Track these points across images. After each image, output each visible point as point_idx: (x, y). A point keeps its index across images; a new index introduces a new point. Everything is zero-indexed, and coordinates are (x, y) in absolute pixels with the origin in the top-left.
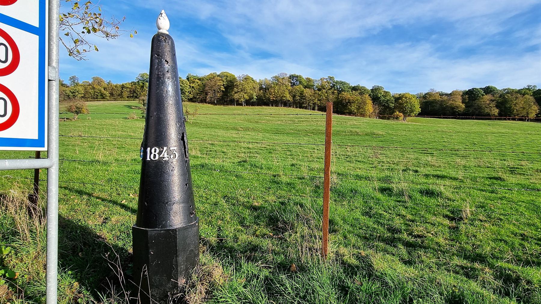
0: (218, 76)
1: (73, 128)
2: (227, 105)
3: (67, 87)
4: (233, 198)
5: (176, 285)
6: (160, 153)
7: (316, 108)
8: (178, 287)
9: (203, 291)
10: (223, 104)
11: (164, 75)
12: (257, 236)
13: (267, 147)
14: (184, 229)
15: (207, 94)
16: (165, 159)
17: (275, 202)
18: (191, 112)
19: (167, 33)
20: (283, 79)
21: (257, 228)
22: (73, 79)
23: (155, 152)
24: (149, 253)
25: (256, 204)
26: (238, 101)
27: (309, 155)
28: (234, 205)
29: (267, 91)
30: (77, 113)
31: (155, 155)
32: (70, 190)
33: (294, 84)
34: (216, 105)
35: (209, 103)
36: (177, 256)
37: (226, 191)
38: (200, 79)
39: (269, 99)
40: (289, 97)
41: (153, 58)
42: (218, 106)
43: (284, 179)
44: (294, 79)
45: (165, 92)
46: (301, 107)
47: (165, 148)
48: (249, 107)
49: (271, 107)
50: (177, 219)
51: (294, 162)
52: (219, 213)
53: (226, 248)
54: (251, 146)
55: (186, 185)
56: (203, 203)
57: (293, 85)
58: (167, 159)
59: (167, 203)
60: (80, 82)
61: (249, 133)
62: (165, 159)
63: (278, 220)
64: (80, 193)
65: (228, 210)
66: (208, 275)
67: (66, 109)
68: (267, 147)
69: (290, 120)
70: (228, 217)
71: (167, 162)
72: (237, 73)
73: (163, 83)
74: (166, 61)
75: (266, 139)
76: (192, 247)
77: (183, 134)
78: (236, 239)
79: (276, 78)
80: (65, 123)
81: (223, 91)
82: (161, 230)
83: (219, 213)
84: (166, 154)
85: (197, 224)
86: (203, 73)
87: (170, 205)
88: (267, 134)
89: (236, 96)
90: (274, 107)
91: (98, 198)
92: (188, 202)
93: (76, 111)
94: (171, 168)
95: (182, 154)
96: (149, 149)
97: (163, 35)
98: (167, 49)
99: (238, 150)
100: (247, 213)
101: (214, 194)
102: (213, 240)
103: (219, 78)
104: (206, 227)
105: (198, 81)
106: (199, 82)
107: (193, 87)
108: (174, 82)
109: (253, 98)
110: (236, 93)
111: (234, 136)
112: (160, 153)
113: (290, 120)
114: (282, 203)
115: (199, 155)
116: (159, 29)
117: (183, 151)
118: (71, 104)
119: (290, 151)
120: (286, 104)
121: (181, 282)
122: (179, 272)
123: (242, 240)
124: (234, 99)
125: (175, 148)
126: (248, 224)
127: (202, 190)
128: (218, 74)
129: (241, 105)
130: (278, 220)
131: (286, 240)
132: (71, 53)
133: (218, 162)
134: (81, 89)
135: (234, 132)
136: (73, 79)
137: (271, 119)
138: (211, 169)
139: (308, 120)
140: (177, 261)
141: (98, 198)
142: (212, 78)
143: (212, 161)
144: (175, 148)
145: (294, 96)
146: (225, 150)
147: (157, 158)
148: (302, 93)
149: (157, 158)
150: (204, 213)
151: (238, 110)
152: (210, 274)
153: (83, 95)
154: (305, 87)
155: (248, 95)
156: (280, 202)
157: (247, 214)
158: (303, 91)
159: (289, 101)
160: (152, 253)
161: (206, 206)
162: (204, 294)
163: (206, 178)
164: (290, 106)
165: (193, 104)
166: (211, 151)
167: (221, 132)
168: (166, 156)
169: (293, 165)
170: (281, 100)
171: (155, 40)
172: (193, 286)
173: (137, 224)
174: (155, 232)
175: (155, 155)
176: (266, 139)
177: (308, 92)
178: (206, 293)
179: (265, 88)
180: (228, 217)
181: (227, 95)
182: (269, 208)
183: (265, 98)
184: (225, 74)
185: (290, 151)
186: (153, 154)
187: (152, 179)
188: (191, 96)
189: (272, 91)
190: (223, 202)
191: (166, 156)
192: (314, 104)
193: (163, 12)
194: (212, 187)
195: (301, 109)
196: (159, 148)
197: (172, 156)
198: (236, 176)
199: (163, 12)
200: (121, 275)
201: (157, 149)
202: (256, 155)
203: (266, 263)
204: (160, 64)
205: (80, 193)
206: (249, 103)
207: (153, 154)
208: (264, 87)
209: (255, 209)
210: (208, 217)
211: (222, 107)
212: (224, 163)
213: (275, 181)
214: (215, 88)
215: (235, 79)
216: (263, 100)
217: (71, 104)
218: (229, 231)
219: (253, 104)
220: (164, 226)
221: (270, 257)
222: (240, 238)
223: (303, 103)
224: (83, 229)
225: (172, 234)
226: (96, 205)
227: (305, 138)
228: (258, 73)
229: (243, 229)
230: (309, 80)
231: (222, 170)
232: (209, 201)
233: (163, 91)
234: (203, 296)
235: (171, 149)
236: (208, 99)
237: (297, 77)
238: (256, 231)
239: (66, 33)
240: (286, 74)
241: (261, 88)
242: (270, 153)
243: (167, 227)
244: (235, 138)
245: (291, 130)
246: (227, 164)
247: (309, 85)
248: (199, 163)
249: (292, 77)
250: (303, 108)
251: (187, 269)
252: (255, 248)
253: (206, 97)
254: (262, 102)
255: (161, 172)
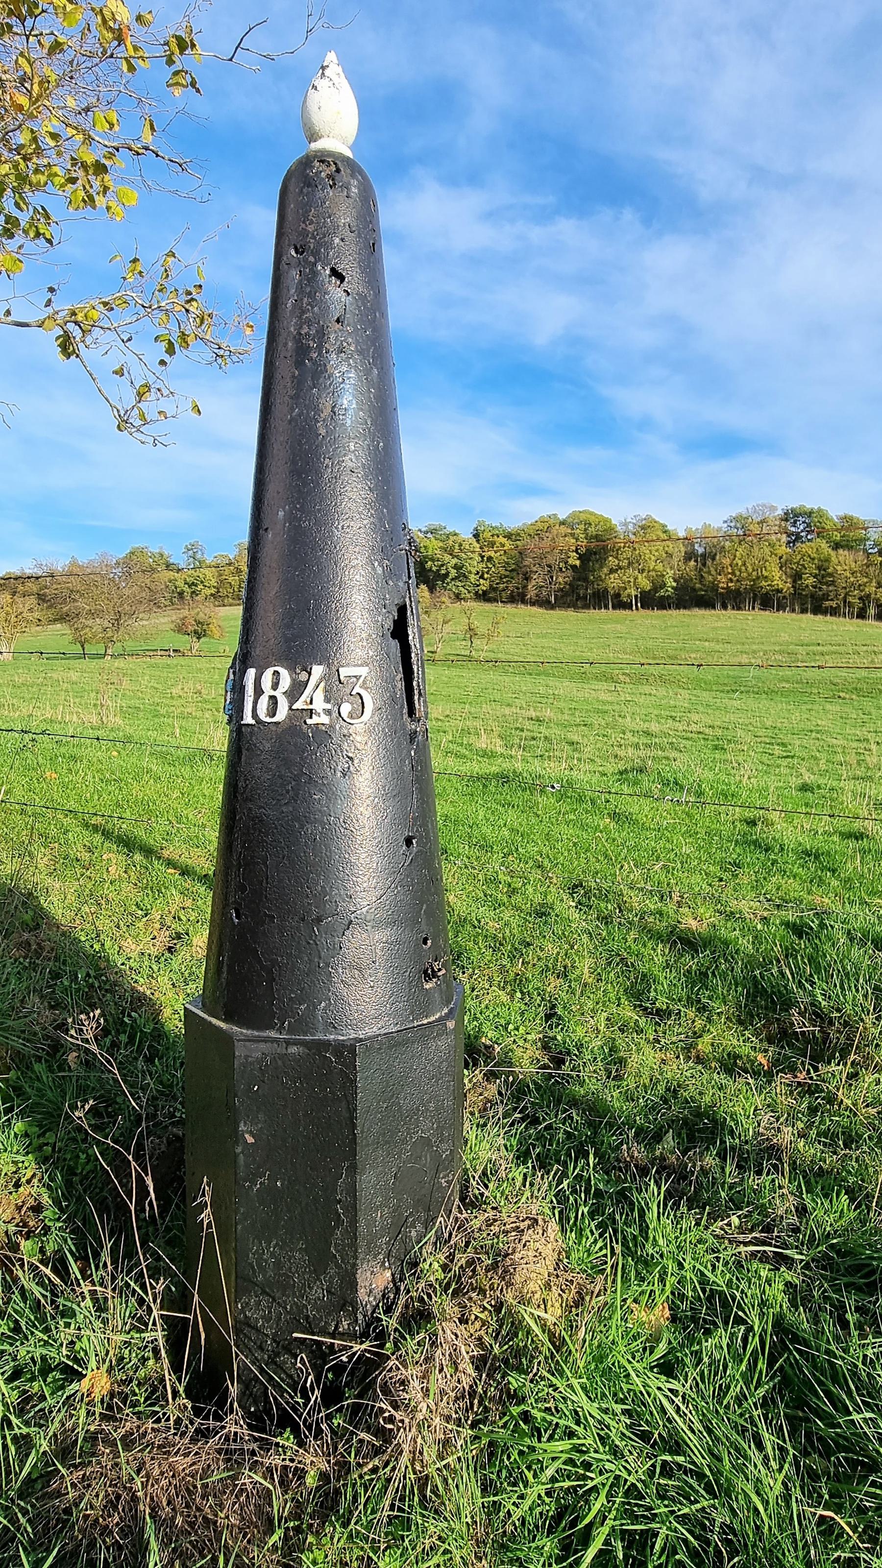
0: (563, 523)
1: (185, 674)
2: (586, 607)
3: (179, 570)
4: (604, 896)
5: (345, 1297)
6: (296, 690)
7: (872, 611)
8: (354, 1304)
9: (467, 1352)
10: (574, 606)
11: (322, 334)
12: (699, 1060)
13: (707, 731)
14: (393, 1043)
15: (527, 578)
16: (315, 720)
17: (764, 920)
18: (482, 630)
19: (348, 153)
20: (762, 522)
21: (699, 1024)
22: (192, 550)
23: (275, 686)
24: (237, 1137)
25: (693, 924)
26: (618, 595)
27: (852, 759)
28: (606, 920)
29: (709, 562)
30: (199, 636)
31: (273, 699)
32: (107, 834)
33: (798, 537)
34: (552, 607)
35: (533, 604)
36: (353, 1169)
37: (579, 865)
38: (509, 536)
39: (714, 588)
40: (778, 580)
41: (284, 267)
42: (558, 613)
43: (788, 832)
44: (801, 523)
45: (327, 412)
46: (818, 610)
47: (318, 671)
48: (649, 612)
49: (718, 612)
50: (363, 991)
51: (808, 778)
52: (551, 949)
53: (574, 1103)
54: (654, 727)
55: (408, 841)
56: (497, 905)
57: (795, 539)
58: (325, 719)
59: (319, 920)
60: (209, 560)
61: (646, 689)
62: (315, 720)
63: (788, 1004)
64: (128, 844)
65: (585, 938)
66: (494, 1266)
67: (172, 626)
68: (707, 731)
69: (781, 652)
70: (585, 967)
71: (322, 735)
72: (618, 509)
73: (319, 372)
74: (335, 273)
75: (701, 709)
76: (426, 1128)
77: (402, 610)
78: (615, 1064)
79: (741, 521)
80: (169, 661)
81: (574, 567)
82: (288, 1043)
83: (551, 949)
84: (319, 696)
85: (451, 1025)
86: (521, 513)
87: (331, 931)
88: (704, 694)
89: (613, 582)
90: (730, 612)
91: (170, 863)
92: (414, 922)
93: (196, 632)
94: (342, 764)
95: (393, 699)
96: (251, 673)
97: (323, 158)
98: (344, 215)
99: (615, 737)
100: (656, 956)
101: (537, 874)
102: (527, 1061)
103: (563, 530)
104: (504, 997)
105: (504, 540)
106: (508, 544)
107: (490, 559)
108: (368, 372)
109: (663, 585)
110: (612, 571)
111: (603, 696)
112: (296, 690)
113: (781, 652)
114: (799, 930)
115: (499, 750)
116: (313, 137)
117: (400, 685)
118: (185, 613)
119: (784, 745)
120: (768, 601)
121: (374, 1280)
122: (362, 1244)
123: (639, 1075)
124: (606, 590)
125: (363, 671)
126: (662, 1003)
127: (498, 857)
128: (562, 516)
129: (627, 606)
130: (788, 1004)
131: (831, 1099)
132: (123, 424)
133: (553, 769)
134: (210, 575)
135: (603, 685)
136: (192, 550)
137: (718, 647)
138: (532, 788)
139: (842, 649)
140: (352, 1190)
141: (170, 863)
142: (543, 530)
143: (536, 766)
144: (363, 671)
145: (797, 577)
146: (575, 738)
147: (282, 714)
148: (823, 567)
149: (282, 714)
150: (497, 943)
151: (617, 622)
152: (501, 1264)
153: (213, 591)
154: (837, 546)
155: (648, 577)
156: (787, 924)
157: (659, 960)
158: (828, 560)
159: (779, 591)
160: (250, 1140)
161: (507, 915)
162: (470, 1370)
163: (512, 817)
164: (781, 607)
165: (488, 606)
166: (534, 739)
167: (565, 687)
168: (319, 704)
169: (805, 788)
170: (753, 589)
171: (293, 188)
172: (419, 1317)
173: (207, 1001)
174: (262, 1046)
175: (273, 699)
176: (701, 709)
177: (844, 563)
178: (480, 1363)
179: (702, 554)
180: (585, 967)
181: (586, 580)
182: (746, 944)
183: (703, 585)
184: (583, 517)
185: (784, 745)
186: (271, 694)
187: (268, 803)
188: (484, 585)
189: (727, 561)
190: (566, 906)
191: (319, 704)
192: (865, 599)
193: (331, 57)
194: (532, 849)
195: (820, 617)
196: (291, 669)
197: (346, 709)
198: (615, 816)
199: (331, 57)
200: (143, 1192)
201: (284, 673)
202: (673, 754)
203: (768, 1229)
204: (310, 285)
205: (128, 844)
206: (651, 600)
207: (271, 694)
208: (701, 551)
209: (686, 942)
210: (512, 958)
211: (570, 613)
212: (574, 773)
213: (754, 840)
214: (550, 560)
215: (611, 529)
216: (694, 590)
217: (185, 613)
218: (588, 1029)
219: (663, 604)
220: (304, 1024)
221: (781, 1196)
222: (634, 1061)
223: (826, 597)
224: (97, 968)
225: (334, 1068)
226: (158, 890)
227: (828, 706)
228: (682, 505)
229: (642, 1022)
230: (849, 523)
231: (567, 791)
232: (518, 899)
233: (318, 411)
234: (466, 1382)
235: (344, 672)
236: (531, 593)
237: (810, 514)
238: (697, 1035)
239: (117, 367)
240: (773, 508)
241: (689, 556)
242: (716, 748)
243: (313, 1030)
244: (604, 703)
245: (780, 681)
246: (584, 776)
247: (847, 536)
248: (494, 769)
249: (791, 516)
250: (824, 612)
251: (398, 1227)
252: (702, 1127)
253: (525, 587)
254: (693, 596)
255: (297, 778)
